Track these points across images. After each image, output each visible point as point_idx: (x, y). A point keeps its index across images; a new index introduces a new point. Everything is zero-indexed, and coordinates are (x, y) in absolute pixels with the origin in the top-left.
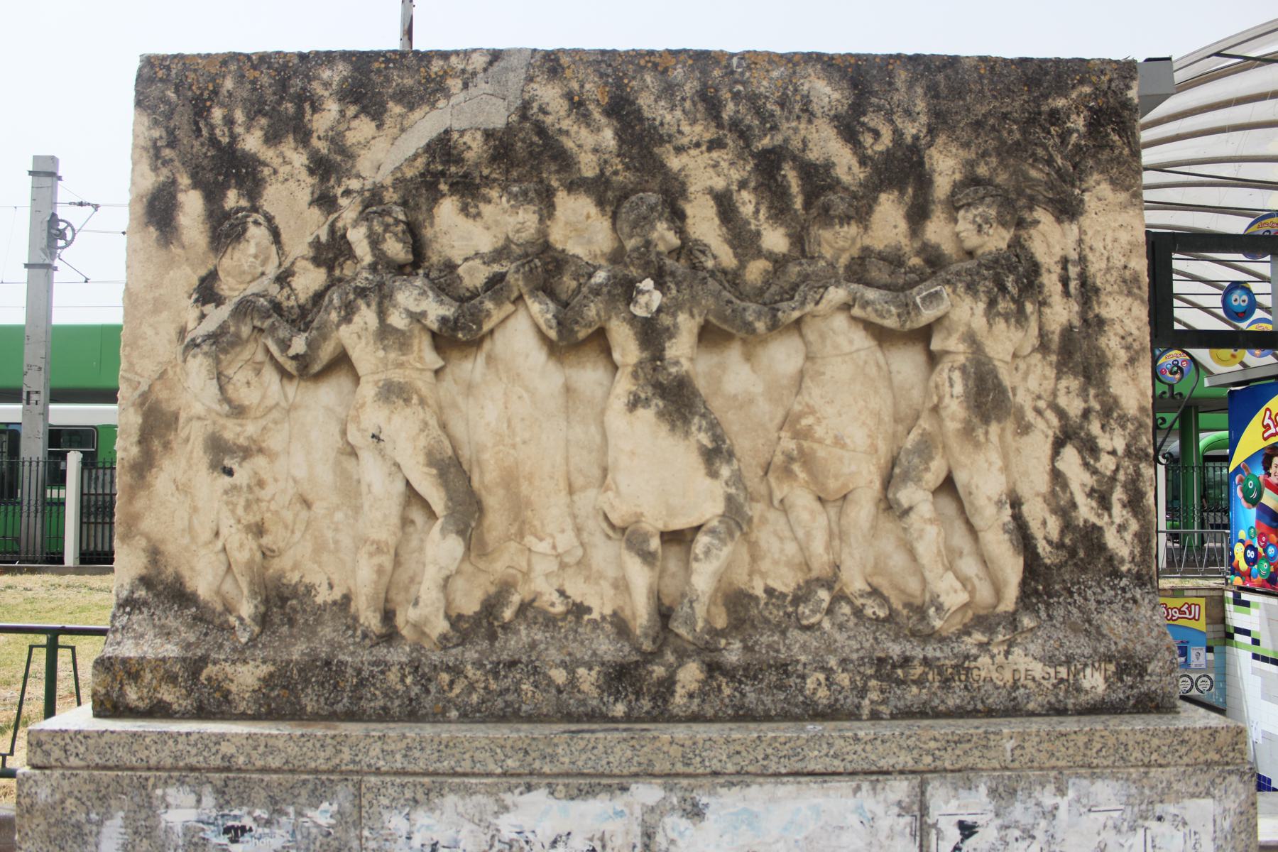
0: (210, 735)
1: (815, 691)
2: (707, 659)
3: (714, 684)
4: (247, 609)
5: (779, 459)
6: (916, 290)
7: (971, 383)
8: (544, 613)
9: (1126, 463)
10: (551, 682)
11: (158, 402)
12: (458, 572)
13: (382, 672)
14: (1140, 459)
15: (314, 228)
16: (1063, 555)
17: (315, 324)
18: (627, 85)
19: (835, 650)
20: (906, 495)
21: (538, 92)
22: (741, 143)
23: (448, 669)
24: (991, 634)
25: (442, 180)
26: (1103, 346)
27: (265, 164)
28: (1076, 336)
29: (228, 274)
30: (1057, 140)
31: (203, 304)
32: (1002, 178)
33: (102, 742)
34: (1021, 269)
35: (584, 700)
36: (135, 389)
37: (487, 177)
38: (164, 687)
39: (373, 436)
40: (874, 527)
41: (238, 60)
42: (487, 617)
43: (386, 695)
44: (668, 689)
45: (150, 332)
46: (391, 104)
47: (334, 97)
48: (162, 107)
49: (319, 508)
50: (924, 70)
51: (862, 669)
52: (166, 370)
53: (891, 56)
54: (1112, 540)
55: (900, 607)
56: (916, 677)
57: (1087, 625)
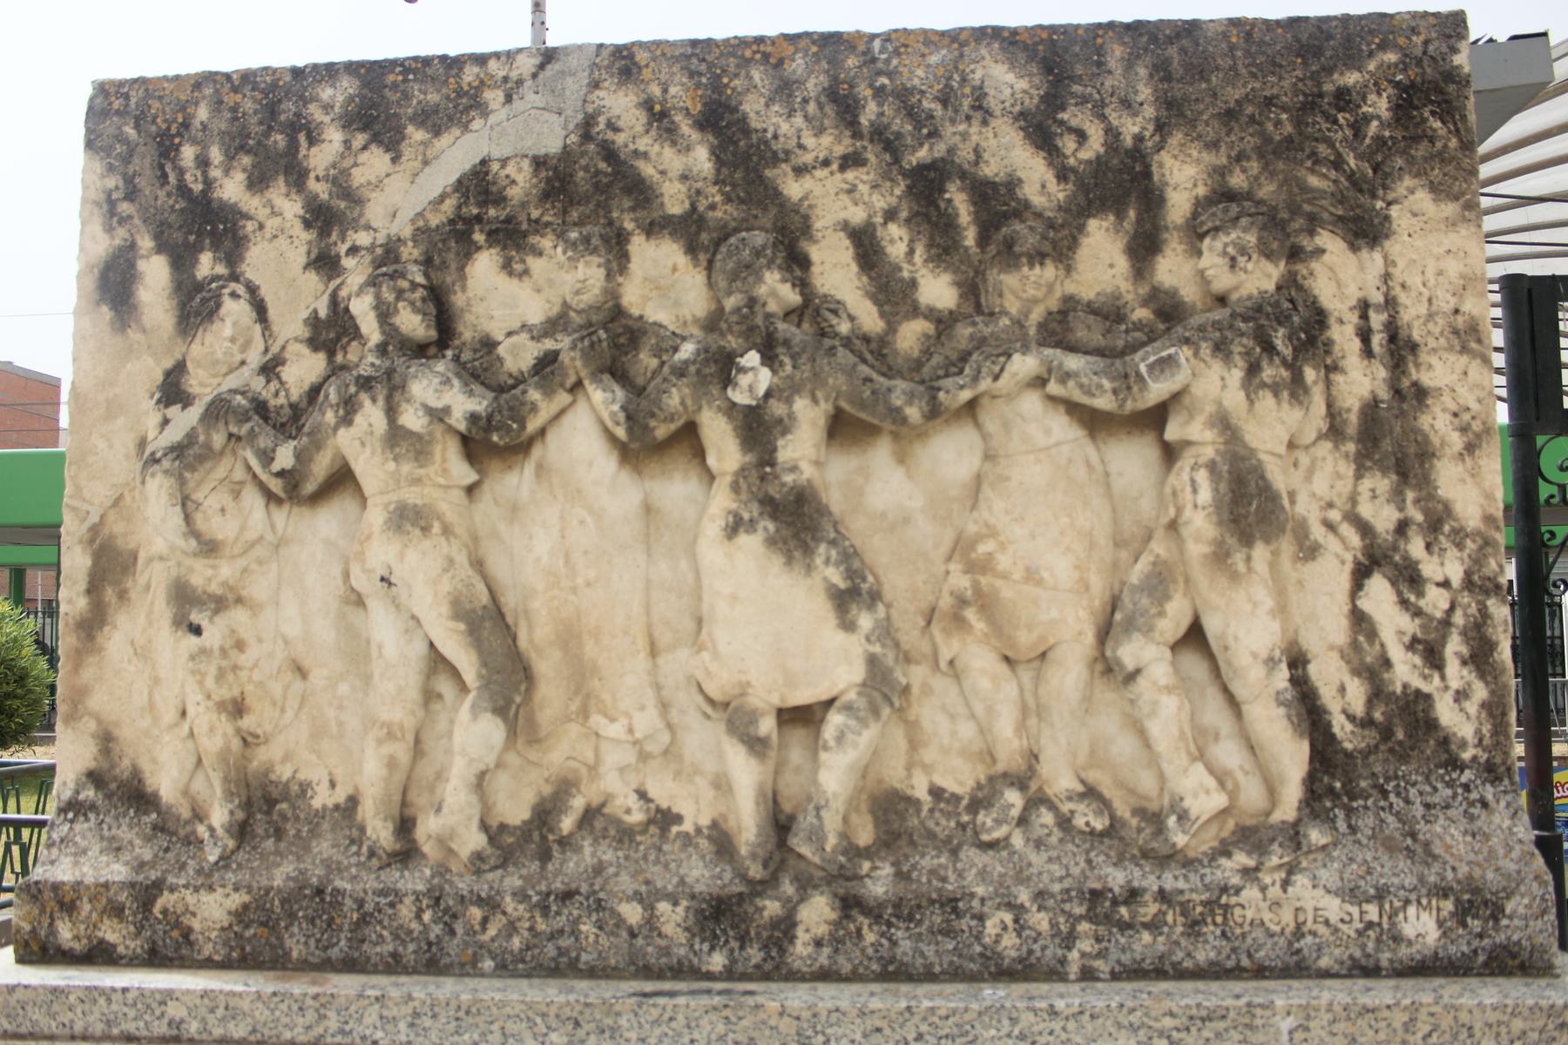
0: (153, 992)
1: (998, 937)
2: (841, 891)
3: (852, 927)
4: (219, 815)
5: (946, 602)
6: (1140, 354)
7: (1223, 487)
8: (618, 822)
9: (1465, 599)
10: (620, 921)
11: (112, 537)
12: (499, 765)
13: (392, 905)
14: (1487, 593)
15: (310, 299)
16: (1372, 736)
17: (306, 429)
18: (726, 86)
19: (1029, 878)
20: (1130, 652)
21: (606, 103)
22: (888, 157)
23: (480, 901)
24: (1261, 855)
25: (477, 228)
26: (1426, 427)
27: (248, 217)
28: (1382, 413)
29: (199, 365)
30: (1349, 132)
31: (167, 406)
32: (1267, 190)
33: (13, 1000)
34: (1296, 319)
35: (668, 947)
36: (83, 520)
37: (537, 221)
38: (107, 922)
39: (383, 579)
40: (1087, 699)
41: (215, 82)
42: (540, 829)
43: (396, 937)
44: (786, 933)
45: (101, 445)
46: (410, 129)
47: (336, 123)
48: (119, 148)
49: (318, 677)
50: (1149, 42)
51: (1067, 907)
52: (121, 497)
53: (1099, 26)
54: (1446, 713)
55: (1127, 815)
56: (1147, 919)
57: (1409, 841)
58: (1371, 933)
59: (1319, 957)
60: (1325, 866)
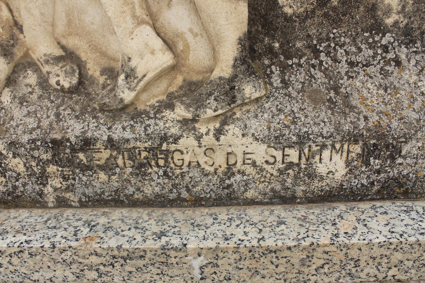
51: (36, 153)
56: (102, 162)
57: (332, 94)
58: (290, 171)
59: (246, 190)
60: (256, 116)
